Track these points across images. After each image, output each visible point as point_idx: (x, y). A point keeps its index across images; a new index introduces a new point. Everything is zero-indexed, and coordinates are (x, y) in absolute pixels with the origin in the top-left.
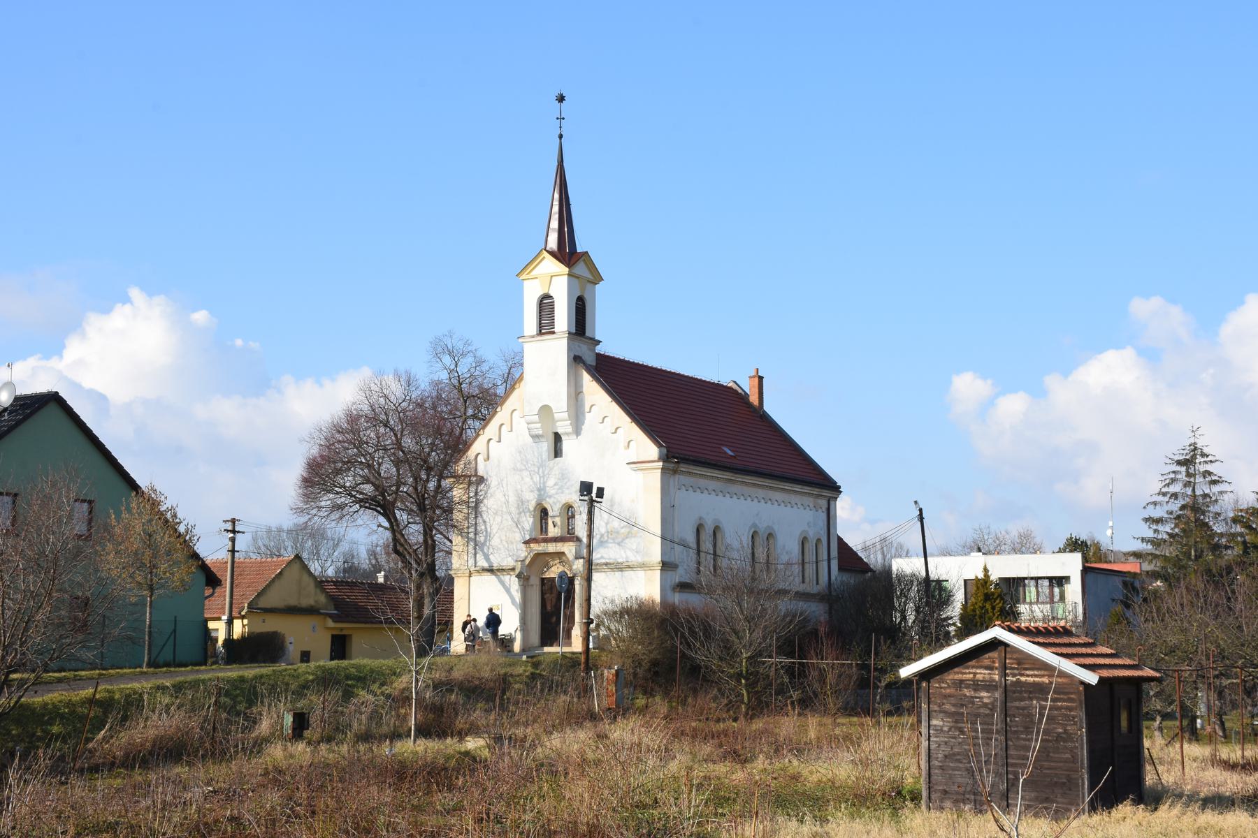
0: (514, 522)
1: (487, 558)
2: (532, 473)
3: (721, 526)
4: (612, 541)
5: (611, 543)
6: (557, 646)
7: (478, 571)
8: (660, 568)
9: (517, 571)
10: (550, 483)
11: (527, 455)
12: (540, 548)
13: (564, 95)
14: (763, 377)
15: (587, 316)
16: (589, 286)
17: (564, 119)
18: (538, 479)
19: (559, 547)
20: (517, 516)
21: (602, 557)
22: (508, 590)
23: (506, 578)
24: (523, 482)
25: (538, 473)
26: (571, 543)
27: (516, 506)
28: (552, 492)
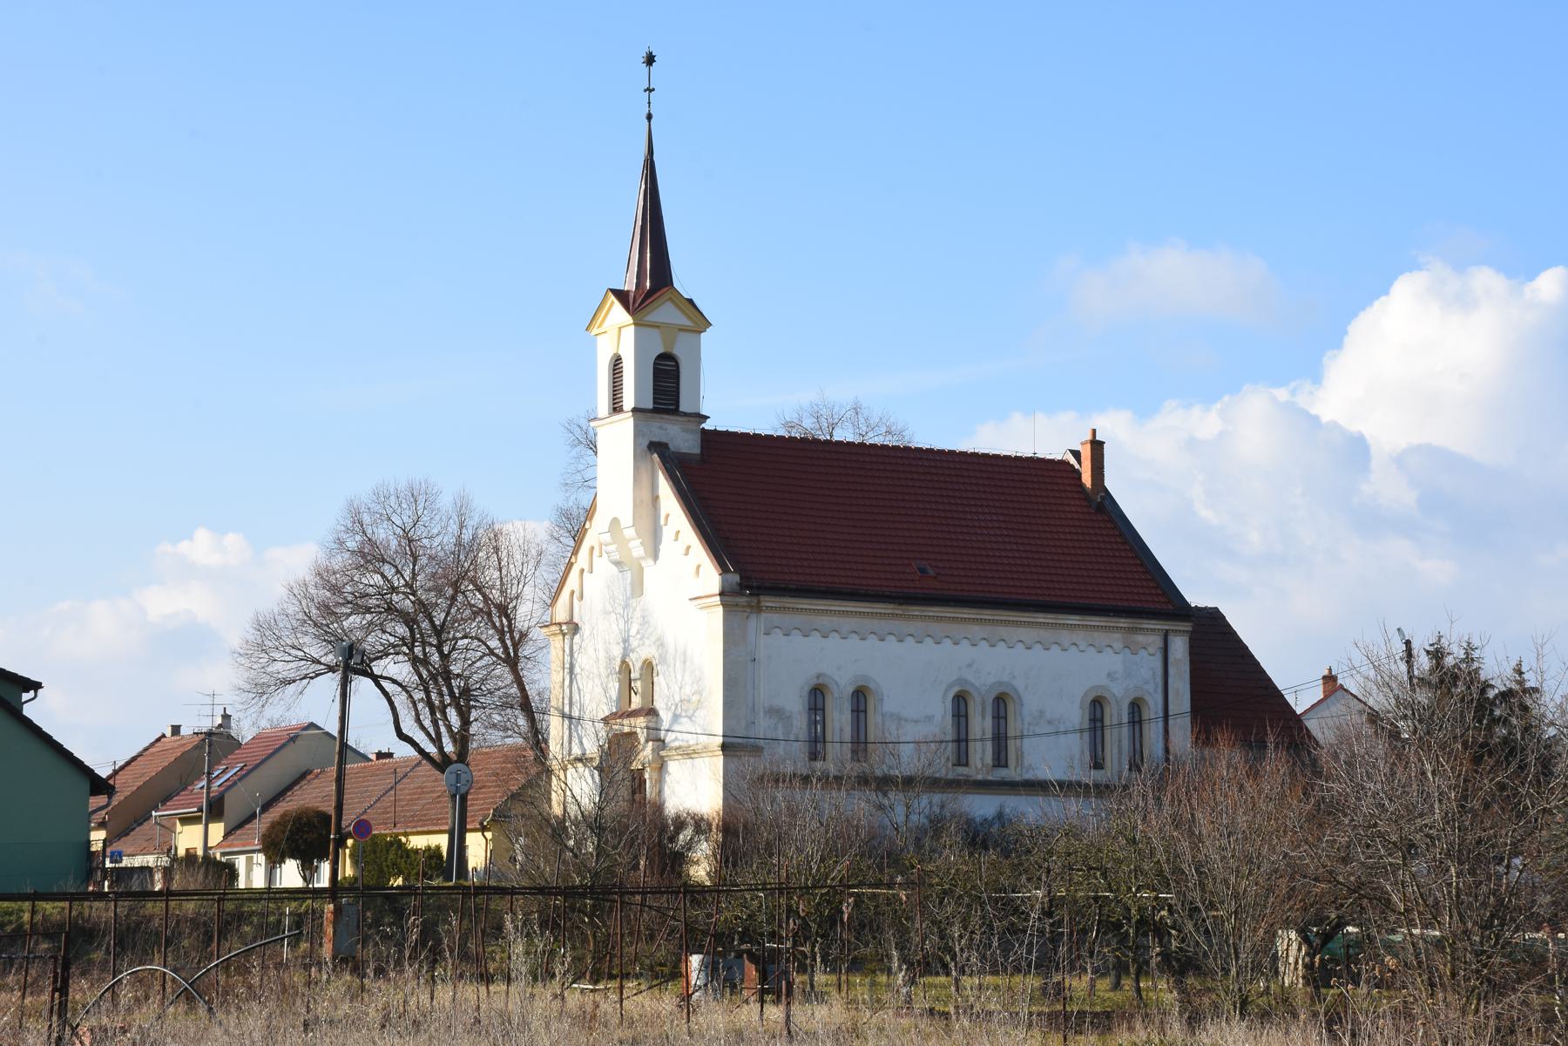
3: (872, 686)
10: (633, 632)
13: (655, 59)
14: (1102, 443)
15: (681, 379)
16: (684, 337)
17: (645, 91)
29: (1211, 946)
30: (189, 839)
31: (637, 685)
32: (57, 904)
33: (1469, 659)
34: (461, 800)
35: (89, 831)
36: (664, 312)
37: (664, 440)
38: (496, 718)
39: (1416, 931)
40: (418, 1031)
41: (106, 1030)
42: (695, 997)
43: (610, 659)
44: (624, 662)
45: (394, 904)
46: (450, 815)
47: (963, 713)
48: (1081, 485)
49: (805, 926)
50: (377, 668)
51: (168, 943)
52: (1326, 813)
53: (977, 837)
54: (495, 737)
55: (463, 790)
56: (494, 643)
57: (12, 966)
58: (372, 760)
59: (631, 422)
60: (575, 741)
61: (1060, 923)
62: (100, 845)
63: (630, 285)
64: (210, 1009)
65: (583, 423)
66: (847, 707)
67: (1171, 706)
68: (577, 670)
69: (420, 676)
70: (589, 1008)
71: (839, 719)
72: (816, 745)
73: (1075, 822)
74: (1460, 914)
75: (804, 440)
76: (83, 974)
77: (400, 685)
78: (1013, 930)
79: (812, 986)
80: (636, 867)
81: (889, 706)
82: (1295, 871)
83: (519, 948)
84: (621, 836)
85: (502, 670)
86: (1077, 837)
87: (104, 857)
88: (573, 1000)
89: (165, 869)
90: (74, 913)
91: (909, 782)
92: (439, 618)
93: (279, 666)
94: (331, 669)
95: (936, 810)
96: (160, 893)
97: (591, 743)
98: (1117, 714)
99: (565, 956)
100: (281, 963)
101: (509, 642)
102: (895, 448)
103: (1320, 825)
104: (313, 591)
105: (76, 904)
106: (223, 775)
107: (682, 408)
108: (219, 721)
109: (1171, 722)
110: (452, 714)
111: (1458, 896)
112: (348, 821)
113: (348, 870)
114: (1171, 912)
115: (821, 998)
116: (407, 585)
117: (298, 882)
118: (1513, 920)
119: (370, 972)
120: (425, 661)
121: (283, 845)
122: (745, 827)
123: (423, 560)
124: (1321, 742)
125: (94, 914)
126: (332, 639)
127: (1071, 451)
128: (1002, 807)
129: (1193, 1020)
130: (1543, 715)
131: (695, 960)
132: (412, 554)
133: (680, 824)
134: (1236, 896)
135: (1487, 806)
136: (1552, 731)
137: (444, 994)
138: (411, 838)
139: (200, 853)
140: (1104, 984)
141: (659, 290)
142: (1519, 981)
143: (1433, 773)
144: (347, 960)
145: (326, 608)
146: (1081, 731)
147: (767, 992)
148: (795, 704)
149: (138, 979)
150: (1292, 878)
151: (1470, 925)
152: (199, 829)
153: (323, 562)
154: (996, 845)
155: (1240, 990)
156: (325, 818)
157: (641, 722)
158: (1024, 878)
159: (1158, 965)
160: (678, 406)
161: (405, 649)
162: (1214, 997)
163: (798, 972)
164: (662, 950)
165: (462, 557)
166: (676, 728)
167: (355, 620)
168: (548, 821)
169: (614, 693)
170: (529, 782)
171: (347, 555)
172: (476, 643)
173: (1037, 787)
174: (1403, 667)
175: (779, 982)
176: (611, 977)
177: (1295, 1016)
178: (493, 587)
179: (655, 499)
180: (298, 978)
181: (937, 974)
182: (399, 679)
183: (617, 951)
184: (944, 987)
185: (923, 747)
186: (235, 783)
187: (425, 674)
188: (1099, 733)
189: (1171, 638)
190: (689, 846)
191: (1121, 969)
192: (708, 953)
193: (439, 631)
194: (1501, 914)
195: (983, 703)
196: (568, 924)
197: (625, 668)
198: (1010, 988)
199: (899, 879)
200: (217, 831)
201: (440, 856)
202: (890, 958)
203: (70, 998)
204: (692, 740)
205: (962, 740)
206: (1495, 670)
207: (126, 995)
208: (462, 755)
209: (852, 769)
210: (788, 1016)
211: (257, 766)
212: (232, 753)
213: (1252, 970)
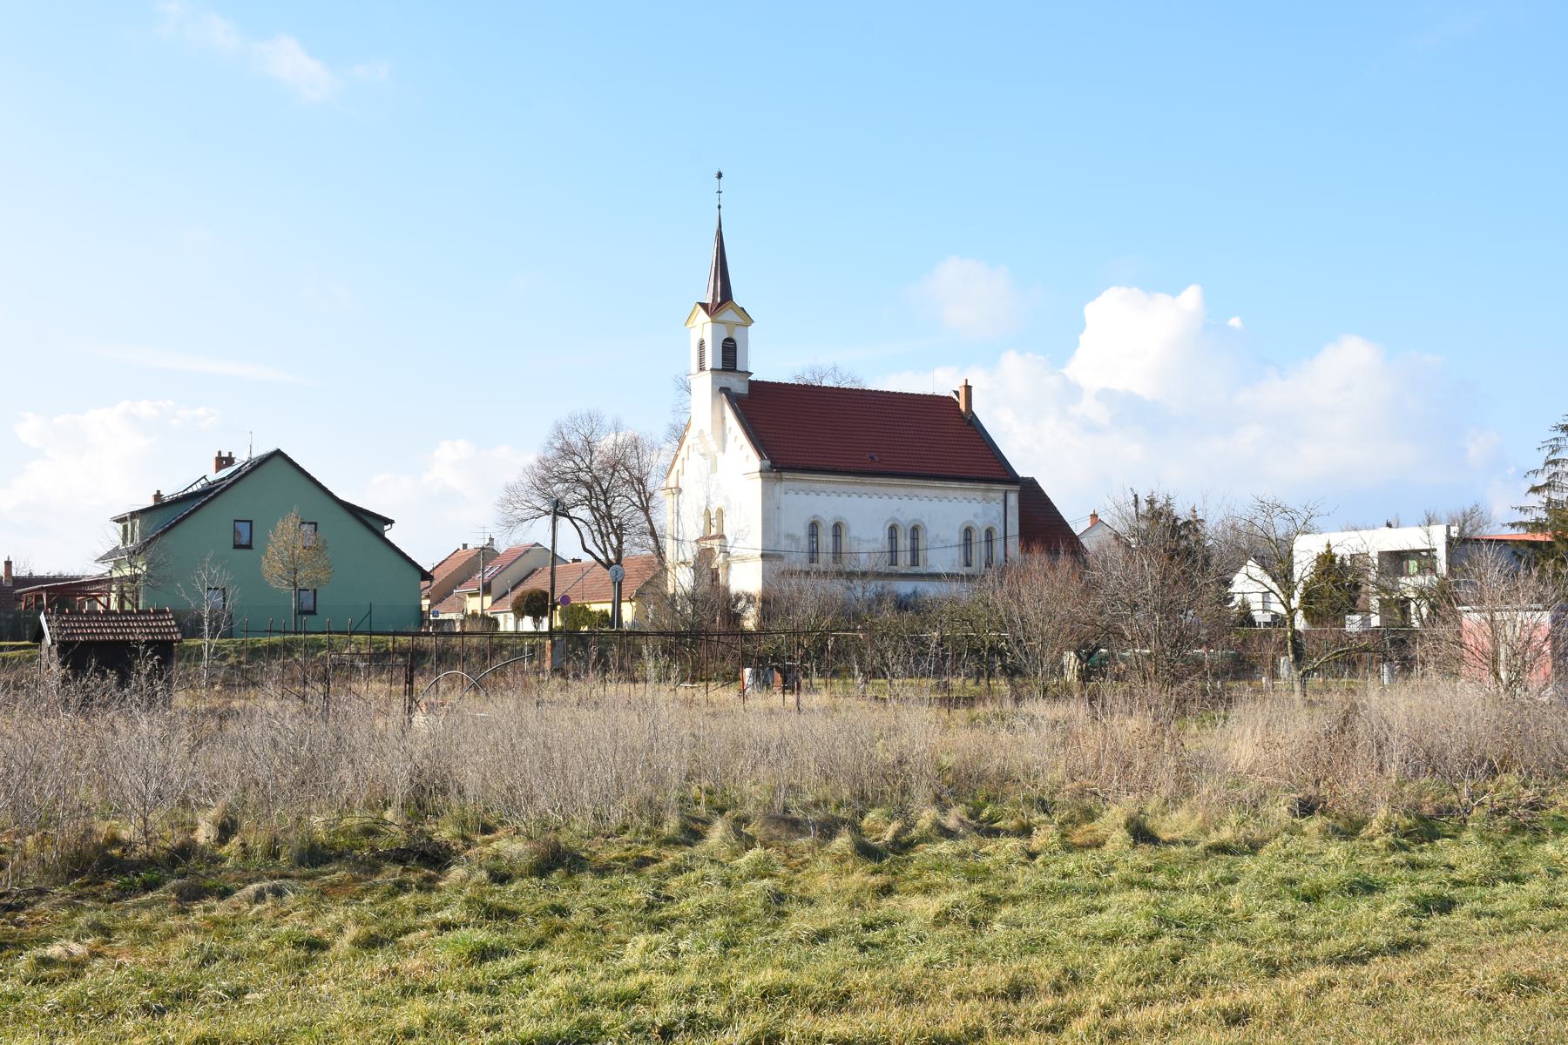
3: (844, 522)
16: (739, 329)
29: (1028, 660)
30: (473, 605)
31: (714, 522)
32: (406, 638)
33: (1168, 504)
34: (619, 585)
35: (421, 599)
36: (728, 315)
37: (728, 386)
38: (637, 540)
39: (1136, 651)
40: (597, 708)
41: (433, 704)
42: (747, 691)
43: (700, 508)
44: (707, 509)
45: (583, 640)
46: (612, 593)
47: (894, 536)
48: (960, 410)
49: (807, 652)
50: (572, 513)
51: (464, 659)
52: (1091, 588)
53: (902, 605)
54: (637, 551)
55: (619, 580)
56: (635, 499)
57: (384, 669)
58: (568, 563)
59: (710, 376)
60: (680, 552)
61: (947, 650)
62: (427, 607)
63: (708, 300)
64: (487, 694)
65: (683, 377)
66: (830, 533)
67: (1008, 532)
68: (681, 514)
69: (595, 517)
70: (690, 697)
71: (826, 540)
72: (813, 555)
73: (956, 595)
74: (1160, 640)
75: (805, 386)
76: (421, 675)
77: (584, 522)
78: (921, 654)
79: (811, 684)
80: (714, 621)
81: (854, 532)
82: (1074, 619)
83: (651, 664)
84: (706, 604)
85: (640, 514)
86: (956, 603)
87: (429, 614)
88: (681, 691)
89: (461, 621)
90: (415, 643)
91: (864, 574)
92: (605, 485)
93: (518, 511)
94: (547, 513)
95: (879, 589)
96: (459, 633)
97: (689, 553)
98: (979, 536)
99: (676, 668)
100: (523, 671)
101: (643, 499)
102: (857, 390)
103: (1088, 595)
104: (536, 470)
105: (415, 638)
106: (491, 570)
107: (738, 369)
108: (487, 541)
109: (1008, 540)
110: (613, 538)
111: (1159, 630)
112: (558, 596)
113: (558, 622)
114: (1007, 643)
115: (816, 691)
116: (587, 467)
117: (532, 629)
118: (1188, 643)
119: (571, 676)
120: (598, 509)
121: (523, 609)
122: (774, 599)
123: (596, 454)
124: (1089, 551)
125: (425, 644)
126: (548, 497)
127: (955, 392)
128: (916, 588)
129: (1018, 699)
130: (1206, 534)
131: (747, 671)
132: (590, 450)
133: (738, 598)
134: (1042, 634)
135: (1176, 582)
136: (1211, 542)
137: (611, 688)
138: (591, 605)
139: (479, 612)
140: (970, 683)
141: (726, 302)
142: (1190, 675)
143: (1148, 565)
144: (558, 670)
145: (544, 480)
146: (959, 546)
147: (787, 688)
148: (802, 532)
149: (450, 679)
150: (1072, 624)
151: (1165, 646)
152: (479, 599)
153: (542, 455)
154: (912, 608)
155: (1043, 684)
156: (545, 594)
157: (716, 542)
158: (927, 626)
159: (1000, 671)
160: (735, 364)
161: (587, 502)
162: (1029, 687)
163: (803, 677)
164: (729, 666)
165: (617, 452)
166: (736, 545)
167: (559, 487)
168: (666, 596)
169: (702, 527)
170: (656, 575)
171: (555, 451)
172: (625, 499)
173: (935, 576)
174: (1134, 509)
175: (793, 683)
176: (702, 680)
177: (1072, 696)
178: (634, 468)
179: (723, 419)
180: (533, 680)
181: (880, 678)
182: (584, 519)
183: (705, 666)
184: (882, 684)
185: (872, 555)
186: (497, 575)
187: (598, 516)
188: (969, 547)
189: (1008, 494)
190: (743, 610)
191: (980, 674)
192: (754, 668)
193: (605, 493)
194: (1182, 639)
195: (906, 530)
196: (678, 652)
197: (707, 512)
198: (919, 685)
199: (859, 627)
200: (488, 600)
201: (608, 615)
202: (853, 669)
203: (414, 687)
204: (745, 552)
205: (894, 551)
206: (1182, 511)
207: (443, 686)
208: (619, 561)
209: (833, 567)
210: (798, 701)
211: (508, 566)
212: (495, 558)
213: (1050, 673)
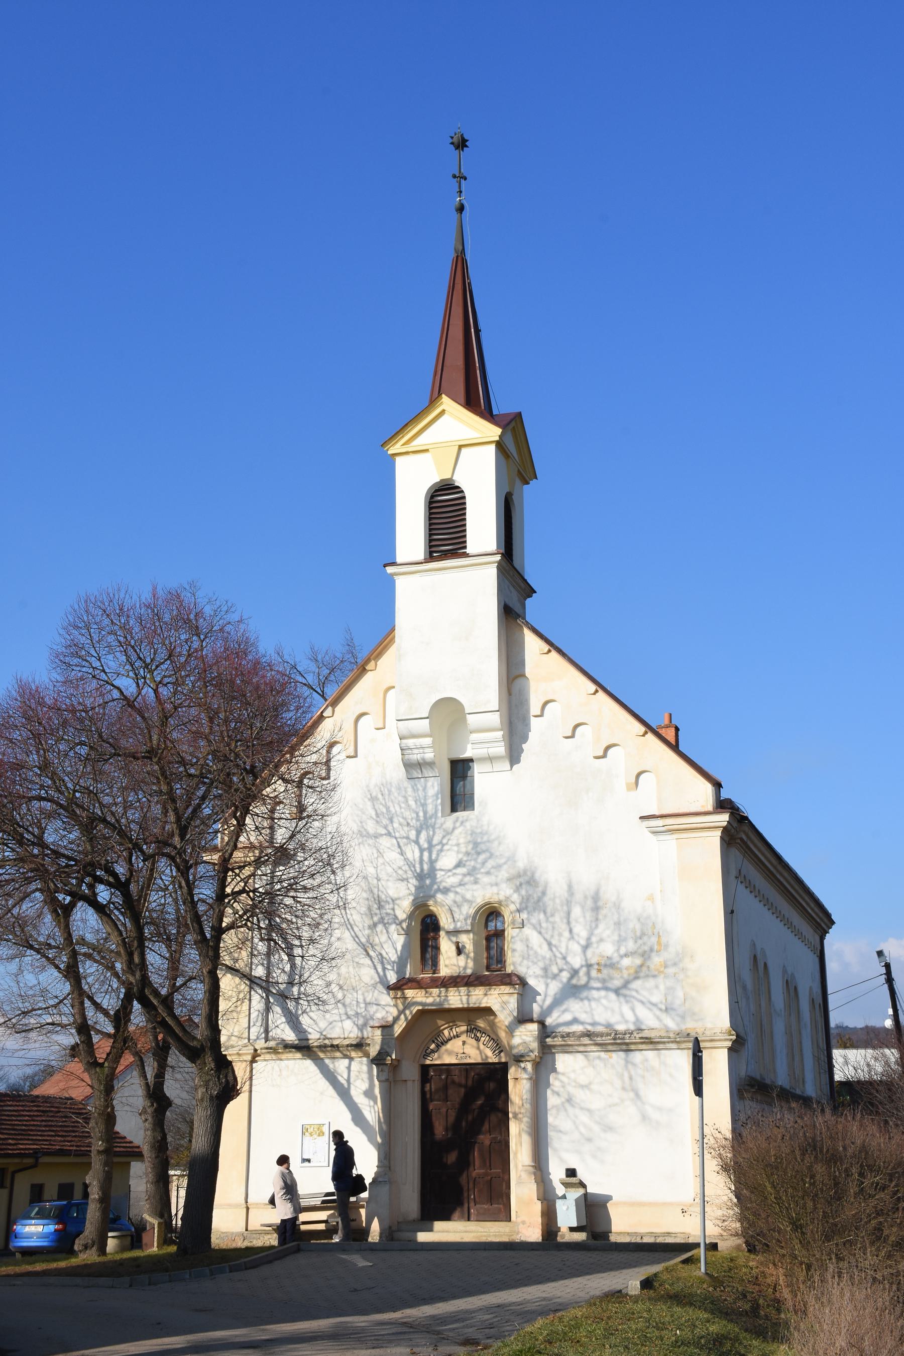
0: (360, 944)
1: (293, 1021)
2: (402, 842)
4: (598, 985)
5: (598, 989)
6: (461, 1218)
7: (273, 1050)
8: (729, 1044)
9: (374, 1051)
10: (446, 861)
11: (390, 804)
12: (430, 1000)
13: (466, 138)
18: (417, 854)
19: (479, 997)
20: (367, 932)
21: (575, 1021)
22: (344, 1093)
23: (340, 1066)
24: (381, 860)
25: (417, 842)
26: (506, 989)
27: (364, 909)
28: (451, 881)
